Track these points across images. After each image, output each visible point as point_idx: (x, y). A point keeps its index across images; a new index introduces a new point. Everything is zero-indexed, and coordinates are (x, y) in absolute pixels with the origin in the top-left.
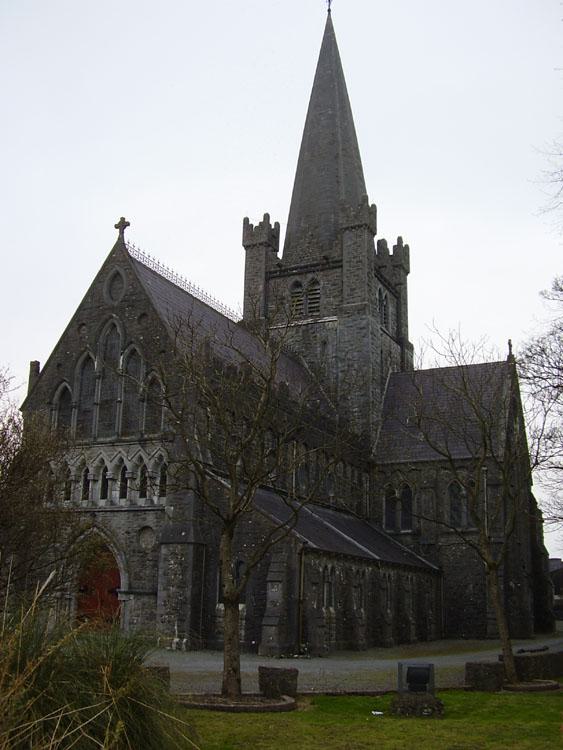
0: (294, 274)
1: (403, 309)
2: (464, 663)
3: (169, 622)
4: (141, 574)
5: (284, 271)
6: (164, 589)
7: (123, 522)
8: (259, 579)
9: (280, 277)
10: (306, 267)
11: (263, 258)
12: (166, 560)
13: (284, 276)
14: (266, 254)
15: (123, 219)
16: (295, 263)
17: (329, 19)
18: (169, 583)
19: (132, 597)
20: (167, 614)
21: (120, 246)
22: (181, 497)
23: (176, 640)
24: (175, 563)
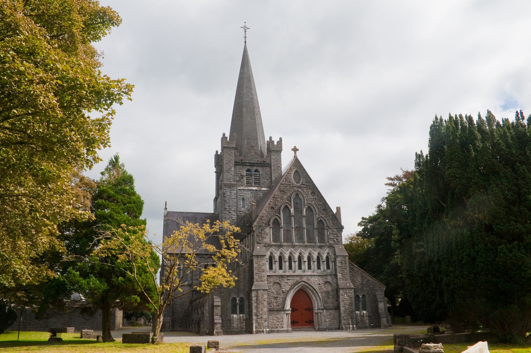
0: (248, 165)
2: (427, 329)
3: (347, 319)
4: (328, 301)
5: (243, 163)
9: (241, 165)
10: (254, 163)
13: (243, 165)
14: (235, 153)
15: (292, 150)
16: (249, 160)
17: (245, 46)
18: (345, 304)
19: (325, 311)
20: (346, 316)
22: (344, 270)
23: (351, 326)
24: (347, 296)
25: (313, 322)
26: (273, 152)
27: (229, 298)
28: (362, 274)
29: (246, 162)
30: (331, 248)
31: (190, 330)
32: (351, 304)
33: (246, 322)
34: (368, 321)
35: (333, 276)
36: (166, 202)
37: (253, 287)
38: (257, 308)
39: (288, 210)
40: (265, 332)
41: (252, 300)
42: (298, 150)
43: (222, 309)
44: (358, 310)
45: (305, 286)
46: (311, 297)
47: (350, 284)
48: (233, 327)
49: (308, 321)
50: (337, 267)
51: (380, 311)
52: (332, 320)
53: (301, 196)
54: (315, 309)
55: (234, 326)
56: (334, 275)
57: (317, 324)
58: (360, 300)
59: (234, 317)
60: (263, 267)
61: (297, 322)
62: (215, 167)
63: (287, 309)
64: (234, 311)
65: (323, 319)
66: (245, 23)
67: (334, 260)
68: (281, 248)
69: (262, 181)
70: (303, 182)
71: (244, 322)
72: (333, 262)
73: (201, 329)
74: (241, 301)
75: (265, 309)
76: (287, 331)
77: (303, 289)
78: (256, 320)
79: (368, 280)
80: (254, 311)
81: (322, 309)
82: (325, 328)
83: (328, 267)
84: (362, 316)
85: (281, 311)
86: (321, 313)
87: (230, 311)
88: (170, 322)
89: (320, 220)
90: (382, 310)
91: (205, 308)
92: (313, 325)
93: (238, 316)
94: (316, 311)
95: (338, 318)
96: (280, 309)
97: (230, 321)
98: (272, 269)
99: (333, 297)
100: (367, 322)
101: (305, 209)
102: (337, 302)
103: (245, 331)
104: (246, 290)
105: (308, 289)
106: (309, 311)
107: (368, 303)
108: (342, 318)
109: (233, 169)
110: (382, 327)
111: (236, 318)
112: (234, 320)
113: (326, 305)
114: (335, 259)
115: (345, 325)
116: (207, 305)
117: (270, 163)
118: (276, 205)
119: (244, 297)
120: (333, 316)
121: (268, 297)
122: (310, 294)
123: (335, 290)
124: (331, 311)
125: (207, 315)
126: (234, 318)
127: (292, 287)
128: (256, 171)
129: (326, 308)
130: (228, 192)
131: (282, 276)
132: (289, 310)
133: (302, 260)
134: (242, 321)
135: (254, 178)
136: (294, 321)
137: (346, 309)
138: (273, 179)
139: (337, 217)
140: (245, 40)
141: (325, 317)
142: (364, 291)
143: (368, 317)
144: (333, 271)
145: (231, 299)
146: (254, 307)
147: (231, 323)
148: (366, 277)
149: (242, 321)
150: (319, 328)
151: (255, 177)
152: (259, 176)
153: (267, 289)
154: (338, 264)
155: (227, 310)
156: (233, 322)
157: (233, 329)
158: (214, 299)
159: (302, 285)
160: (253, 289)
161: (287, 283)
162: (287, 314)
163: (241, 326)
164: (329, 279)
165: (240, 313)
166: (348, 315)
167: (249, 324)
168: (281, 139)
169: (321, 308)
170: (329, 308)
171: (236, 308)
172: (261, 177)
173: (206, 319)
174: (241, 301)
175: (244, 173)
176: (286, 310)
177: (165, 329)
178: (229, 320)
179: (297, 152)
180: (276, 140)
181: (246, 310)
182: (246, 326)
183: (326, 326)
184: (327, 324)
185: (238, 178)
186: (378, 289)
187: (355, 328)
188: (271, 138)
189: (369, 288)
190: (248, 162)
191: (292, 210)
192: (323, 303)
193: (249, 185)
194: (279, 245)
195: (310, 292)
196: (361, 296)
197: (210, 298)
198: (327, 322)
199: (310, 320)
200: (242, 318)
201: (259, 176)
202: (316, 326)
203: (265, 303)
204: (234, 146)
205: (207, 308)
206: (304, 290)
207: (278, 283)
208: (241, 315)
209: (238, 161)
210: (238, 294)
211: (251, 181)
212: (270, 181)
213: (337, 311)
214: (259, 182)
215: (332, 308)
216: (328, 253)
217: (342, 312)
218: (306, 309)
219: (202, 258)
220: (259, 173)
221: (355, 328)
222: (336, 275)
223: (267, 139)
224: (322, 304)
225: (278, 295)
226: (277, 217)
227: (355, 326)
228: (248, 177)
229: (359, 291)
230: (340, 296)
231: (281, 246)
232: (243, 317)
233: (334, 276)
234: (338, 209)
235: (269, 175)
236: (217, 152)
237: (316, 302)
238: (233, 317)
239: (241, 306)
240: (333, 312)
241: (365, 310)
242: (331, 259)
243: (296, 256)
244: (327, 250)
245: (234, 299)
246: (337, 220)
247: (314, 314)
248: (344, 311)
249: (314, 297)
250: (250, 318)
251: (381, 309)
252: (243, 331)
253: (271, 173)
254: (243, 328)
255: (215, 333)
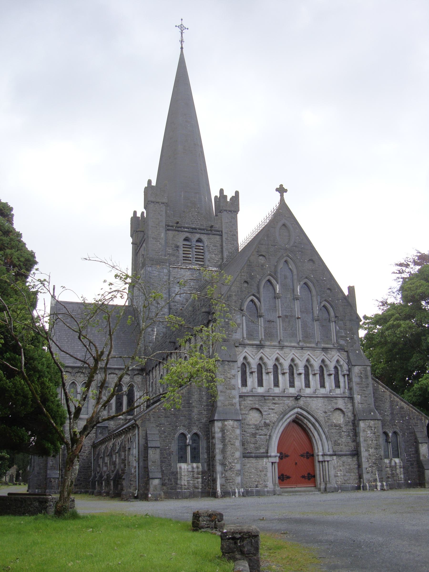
1: (134, 262)
4: (339, 441)
6: (366, 450)
7: (320, 405)
8: (408, 442)
11: (164, 213)
12: (364, 431)
15: (277, 190)
19: (335, 457)
20: (370, 467)
21: (283, 205)
24: (371, 433)
25: (314, 476)
26: (225, 213)
27: (174, 434)
28: (391, 397)
29: (183, 225)
30: (342, 352)
31: (96, 491)
32: (378, 447)
33: (202, 478)
34: (402, 476)
35: (346, 399)
36: (54, 286)
37: (216, 415)
38: (223, 451)
39: (271, 287)
40: (237, 495)
41: (213, 438)
42: (286, 191)
43: (161, 454)
44: (387, 457)
45: (301, 415)
46: (311, 435)
47: (375, 413)
48: (181, 485)
49: (306, 475)
50: (354, 384)
51: (422, 458)
52: (347, 474)
53: (293, 265)
54: (318, 455)
55: (183, 484)
56: (348, 397)
57: (322, 481)
58: (390, 441)
59: (183, 467)
60: (233, 382)
61: (288, 477)
62: (132, 236)
63: (273, 454)
64: (182, 457)
65: (332, 473)
66: (182, 20)
67: (348, 373)
68: (262, 351)
69: (207, 256)
70: (295, 242)
71: (200, 476)
72: (346, 376)
73: (124, 489)
74: (195, 440)
75: (238, 454)
76: (274, 493)
77: (297, 420)
78: (222, 474)
79: (402, 408)
80: (218, 457)
81: (331, 455)
82: (335, 488)
83: (338, 385)
84: (393, 468)
85: (263, 457)
86: (328, 461)
87: (175, 457)
88: (59, 478)
89: (324, 306)
90: (425, 457)
91: (131, 452)
92: (315, 482)
93: (190, 467)
94: (321, 459)
95: (356, 471)
96: (260, 455)
97: (175, 475)
98: (246, 386)
99: (349, 435)
100: (401, 478)
101: (299, 287)
102: (354, 444)
103: (202, 492)
104: (203, 421)
105: (305, 421)
106: (308, 458)
107: (402, 445)
108: (364, 471)
109: (163, 235)
110: (426, 485)
111: (186, 470)
112: (183, 474)
113: (337, 448)
114: (349, 370)
115: (369, 482)
116: (134, 447)
117: (220, 229)
118: (252, 278)
119: (199, 433)
120: (348, 467)
121: (241, 433)
122: (310, 429)
123: (351, 423)
124: (344, 458)
125: (135, 464)
126: (183, 470)
127: (281, 416)
128: (199, 240)
129: (337, 453)
130: (155, 272)
131: (264, 397)
132: (275, 456)
133: (295, 371)
134: (196, 475)
135: (196, 252)
136: (282, 475)
137: (370, 455)
138: (226, 254)
139: (350, 301)
140: (182, 45)
141: (334, 468)
142: (395, 425)
143: (402, 469)
144: (346, 391)
145: (177, 436)
146: (217, 451)
147: (177, 479)
148: (397, 402)
149: (196, 475)
150: (325, 488)
151: (197, 250)
152: (202, 249)
153: (241, 419)
154: (355, 379)
155: (170, 455)
156: (181, 478)
157: (181, 488)
158: (148, 435)
159: (297, 413)
160: (216, 418)
161: (273, 409)
162: (272, 463)
163: (194, 484)
164: (341, 404)
165: (192, 462)
166: (374, 465)
167: (209, 480)
168: (237, 193)
169: (328, 453)
170: (343, 453)
171: (186, 453)
172: (206, 250)
173: (133, 471)
174: (195, 440)
175: (181, 243)
176: (270, 456)
177: (52, 489)
178: (173, 473)
179: (285, 194)
180: (229, 194)
181: (203, 456)
182: (202, 483)
183: (337, 484)
184: (340, 480)
185: (171, 250)
186: (416, 421)
187: (385, 487)
188: (222, 191)
189: (403, 420)
190: (186, 226)
191: (278, 287)
192: (332, 444)
193: (187, 262)
194: (257, 345)
195: (310, 425)
196: (390, 434)
197: (140, 434)
198: (338, 476)
199: (309, 474)
200: (196, 470)
201: (202, 249)
202: (320, 484)
203: (238, 443)
204: (165, 201)
205: (135, 451)
206: (300, 422)
207: (258, 409)
208: (195, 465)
209: (171, 224)
210: (189, 428)
211: (190, 256)
212: (220, 256)
213: (355, 459)
214: (203, 259)
215: (347, 453)
216: (338, 361)
217: (364, 460)
218: (302, 456)
219: (112, 375)
220: (204, 244)
221: (385, 487)
222: (351, 398)
223: (215, 193)
224: (330, 447)
225: (258, 430)
226: (254, 298)
227: (385, 483)
228: (185, 249)
229: (388, 425)
230: (359, 433)
231: (260, 346)
232: (198, 467)
233: (349, 399)
234: (351, 289)
235: (219, 247)
236: (150, 182)
237: (320, 442)
238: (180, 468)
239: (195, 448)
240: (349, 460)
241: (398, 457)
242: (342, 371)
243: (286, 364)
244: (336, 355)
245: (183, 435)
246: (351, 306)
247: (317, 464)
248: (368, 459)
249: (316, 434)
250: (209, 469)
251: (423, 455)
252: (199, 492)
253: (222, 245)
254: (197, 488)
255: (150, 495)
